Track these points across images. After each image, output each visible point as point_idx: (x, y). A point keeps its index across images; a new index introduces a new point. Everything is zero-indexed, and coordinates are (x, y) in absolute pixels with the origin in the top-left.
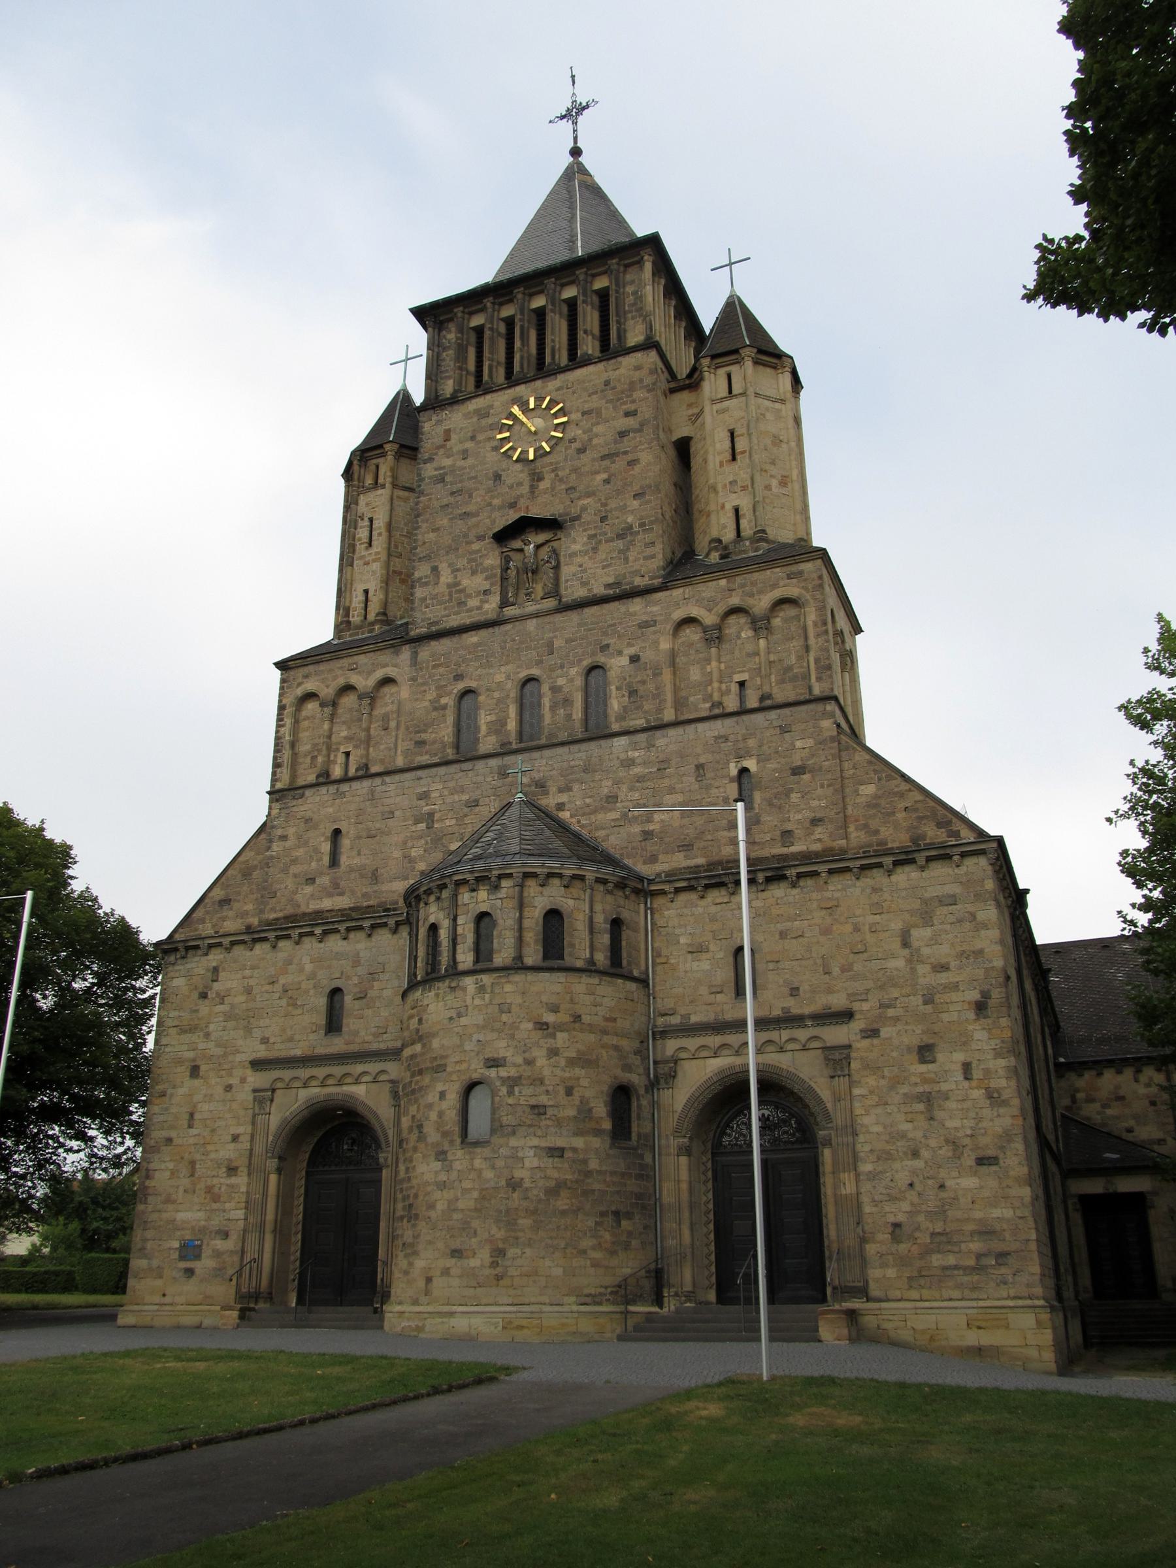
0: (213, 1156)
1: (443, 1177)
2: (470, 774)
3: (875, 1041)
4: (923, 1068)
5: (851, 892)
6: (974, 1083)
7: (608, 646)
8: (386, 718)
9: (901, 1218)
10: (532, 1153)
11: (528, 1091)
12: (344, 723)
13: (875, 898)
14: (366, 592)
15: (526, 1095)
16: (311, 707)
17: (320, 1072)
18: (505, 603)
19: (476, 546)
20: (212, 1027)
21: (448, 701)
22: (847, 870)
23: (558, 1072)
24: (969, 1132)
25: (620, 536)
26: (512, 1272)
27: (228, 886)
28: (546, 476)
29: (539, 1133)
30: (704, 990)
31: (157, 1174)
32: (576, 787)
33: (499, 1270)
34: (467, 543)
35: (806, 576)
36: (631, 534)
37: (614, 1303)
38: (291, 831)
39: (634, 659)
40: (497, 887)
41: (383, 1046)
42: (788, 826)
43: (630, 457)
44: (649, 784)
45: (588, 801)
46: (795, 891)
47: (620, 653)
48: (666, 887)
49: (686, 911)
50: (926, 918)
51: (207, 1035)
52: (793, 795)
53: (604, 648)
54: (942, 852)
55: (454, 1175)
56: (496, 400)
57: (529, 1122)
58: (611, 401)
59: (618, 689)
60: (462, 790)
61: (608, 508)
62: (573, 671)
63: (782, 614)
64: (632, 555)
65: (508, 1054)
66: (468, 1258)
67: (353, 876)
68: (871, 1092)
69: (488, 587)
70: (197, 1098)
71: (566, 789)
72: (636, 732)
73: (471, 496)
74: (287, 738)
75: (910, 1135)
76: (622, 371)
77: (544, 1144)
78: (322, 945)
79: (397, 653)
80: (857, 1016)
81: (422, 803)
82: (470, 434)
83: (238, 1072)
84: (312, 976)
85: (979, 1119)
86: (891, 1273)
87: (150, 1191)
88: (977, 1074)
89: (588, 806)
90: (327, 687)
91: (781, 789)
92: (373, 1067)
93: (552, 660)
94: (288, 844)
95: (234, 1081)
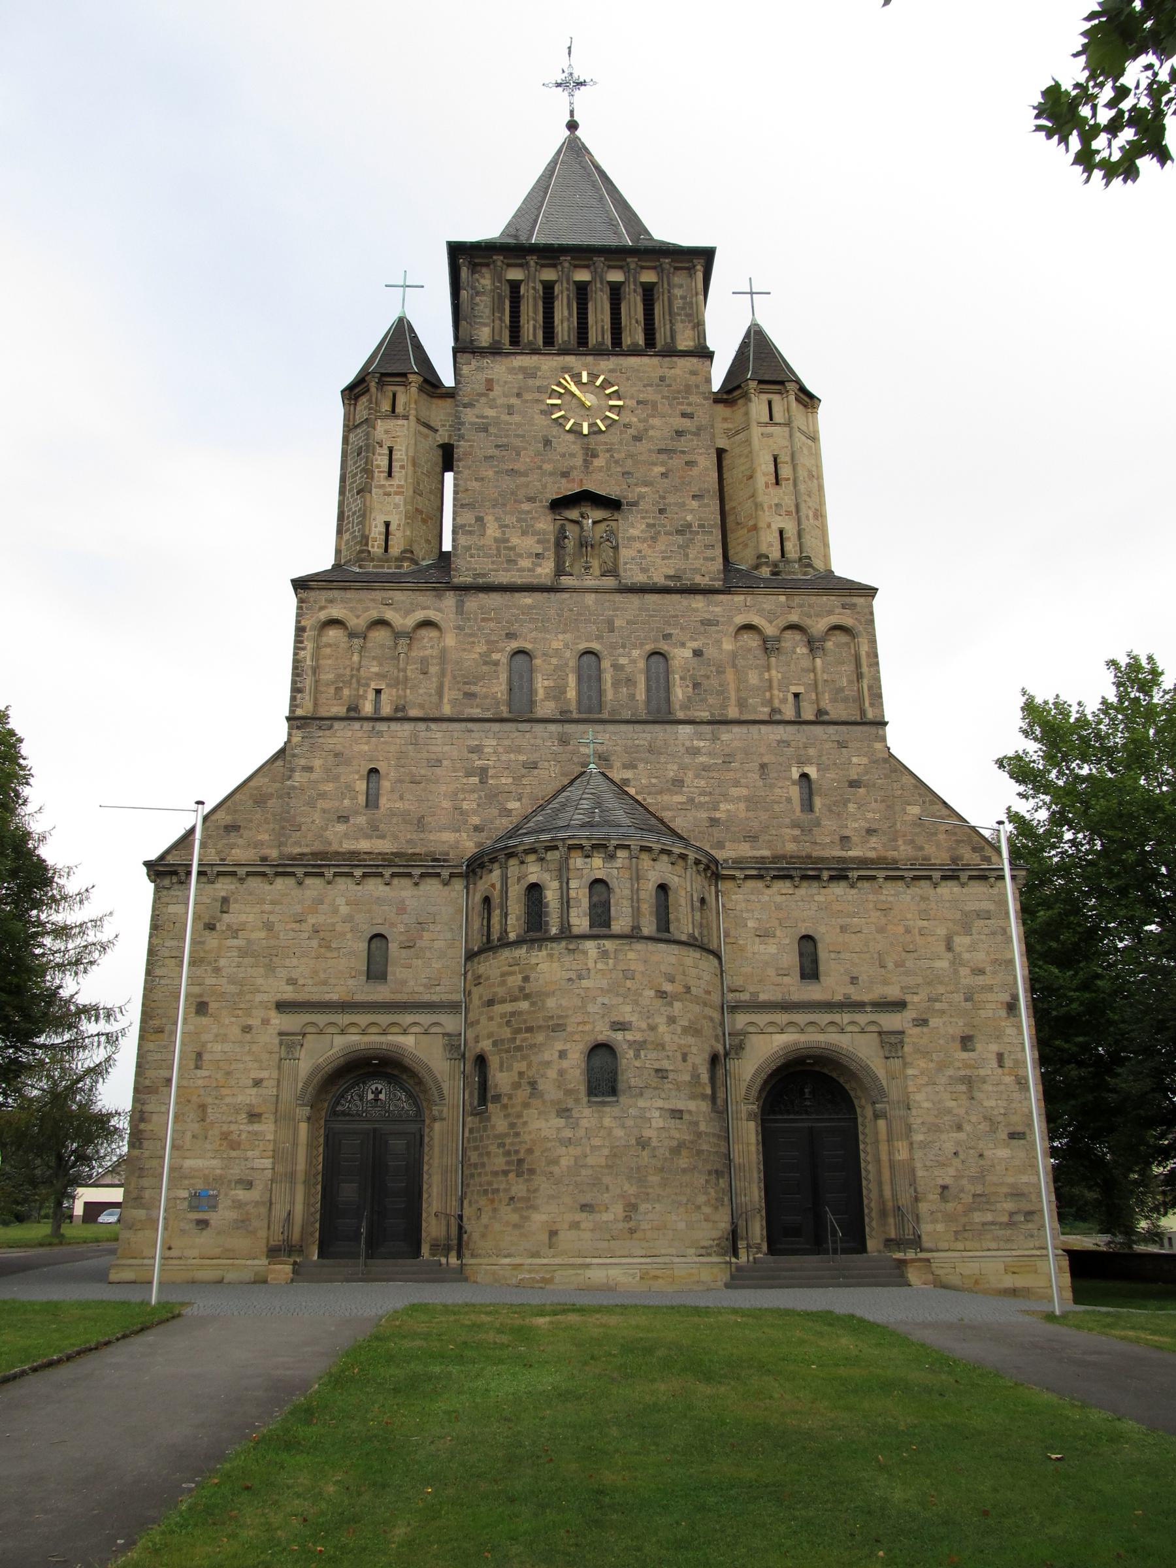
0: (228, 1100)
1: (568, 1133)
2: (528, 735)
3: (925, 1029)
4: (965, 1055)
5: (903, 899)
6: (1006, 1071)
7: (670, 635)
8: (424, 662)
9: (948, 1181)
10: (657, 1114)
11: (652, 1055)
12: (374, 658)
13: (923, 906)
14: (387, 524)
15: (651, 1059)
16: (333, 634)
17: (363, 1019)
18: (560, 571)
19: (526, 507)
20: (222, 962)
21: (501, 657)
22: (902, 878)
23: (676, 1038)
24: (1002, 1111)
25: (678, 532)
26: (645, 1226)
27: (235, 811)
28: (601, 455)
29: (663, 1096)
30: (771, 972)
31: (155, 1117)
32: (641, 766)
33: (632, 1224)
34: (515, 501)
35: (859, 609)
36: (691, 532)
37: (719, 1254)
38: (317, 763)
39: (697, 653)
40: (612, 857)
41: (435, 998)
42: (847, 833)
43: (687, 458)
44: (715, 774)
45: (654, 781)
46: (854, 891)
47: (683, 645)
48: (738, 873)
49: (753, 897)
50: (967, 930)
51: (217, 970)
52: (850, 805)
53: (667, 637)
54: (981, 873)
55: (581, 1133)
56: (548, 364)
57: (654, 1085)
58: (667, 398)
59: (681, 678)
60: (519, 750)
61: (667, 501)
62: (636, 653)
63: (833, 639)
64: (692, 553)
65: (634, 1019)
66: (600, 1212)
67: (394, 820)
68: (922, 1073)
69: (540, 551)
70: (206, 1037)
71: (631, 766)
72: (702, 723)
73: (518, 454)
74: (309, 662)
75: (955, 1111)
76: (677, 371)
77: (667, 1106)
78: (360, 887)
79: (439, 597)
80: (909, 1007)
81: (474, 756)
82: (515, 391)
83: (259, 1013)
84: (348, 919)
85: (1010, 1101)
86: (940, 1227)
87: (146, 1135)
88: (1008, 1063)
89: (654, 785)
90: (358, 617)
91: (838, 798)
92: (425, 1019)
93: (614, 638)
94: (314, 776)
95: (255, 1022)
